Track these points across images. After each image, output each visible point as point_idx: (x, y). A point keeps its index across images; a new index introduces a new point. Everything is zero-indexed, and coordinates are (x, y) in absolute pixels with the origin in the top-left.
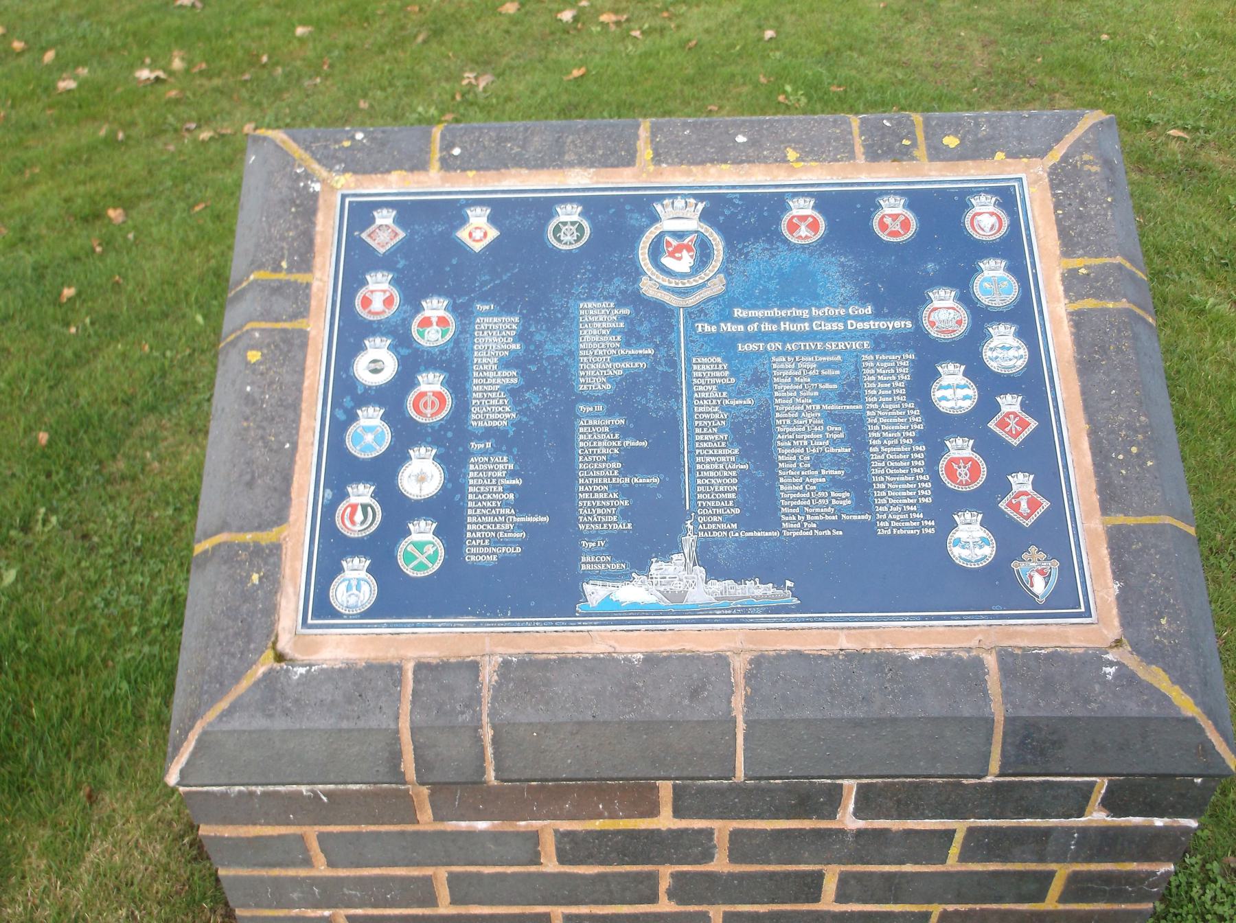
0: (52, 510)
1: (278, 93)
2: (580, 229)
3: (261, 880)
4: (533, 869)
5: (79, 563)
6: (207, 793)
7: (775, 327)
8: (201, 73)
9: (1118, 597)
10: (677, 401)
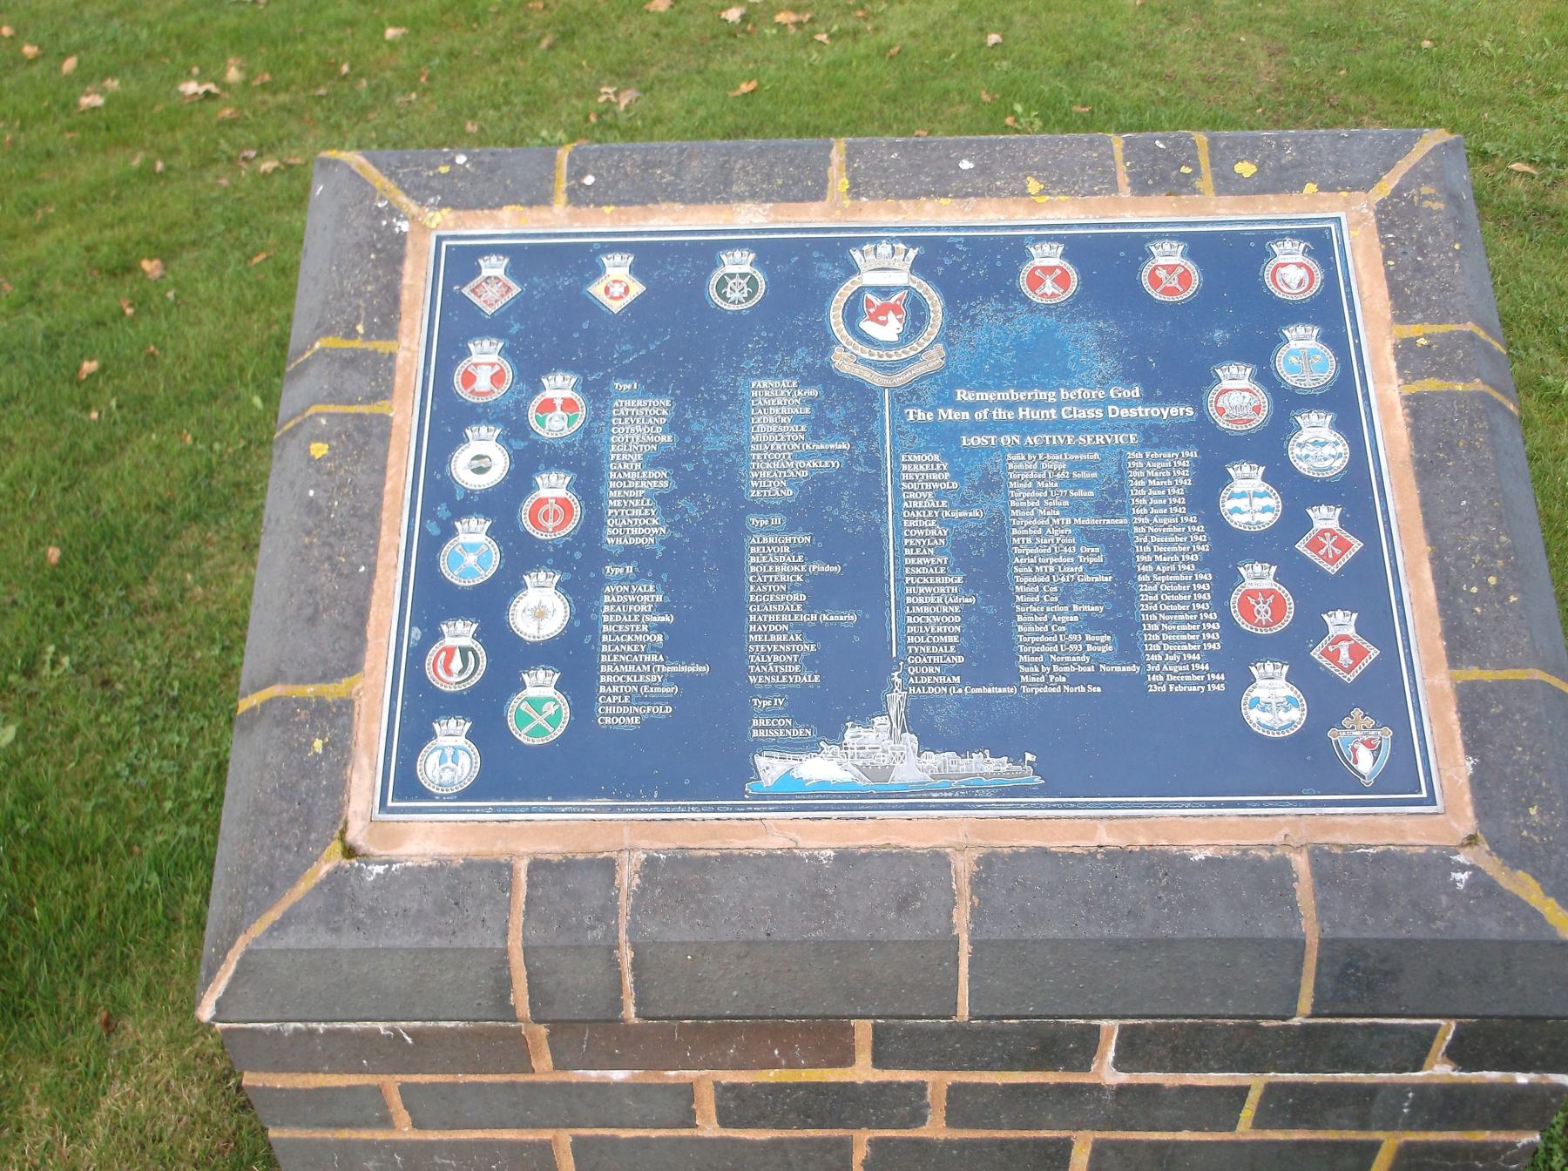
0: (63, 649)
1: (363, 112)
2: (753, 283)
3: (324, 1144)
4: (685, 1132)
5: (97, 717)
6: (252, 1030)
7: (1010, 415)
8: (264, 86)
9: (1472, 778)
10: (880, 512)
